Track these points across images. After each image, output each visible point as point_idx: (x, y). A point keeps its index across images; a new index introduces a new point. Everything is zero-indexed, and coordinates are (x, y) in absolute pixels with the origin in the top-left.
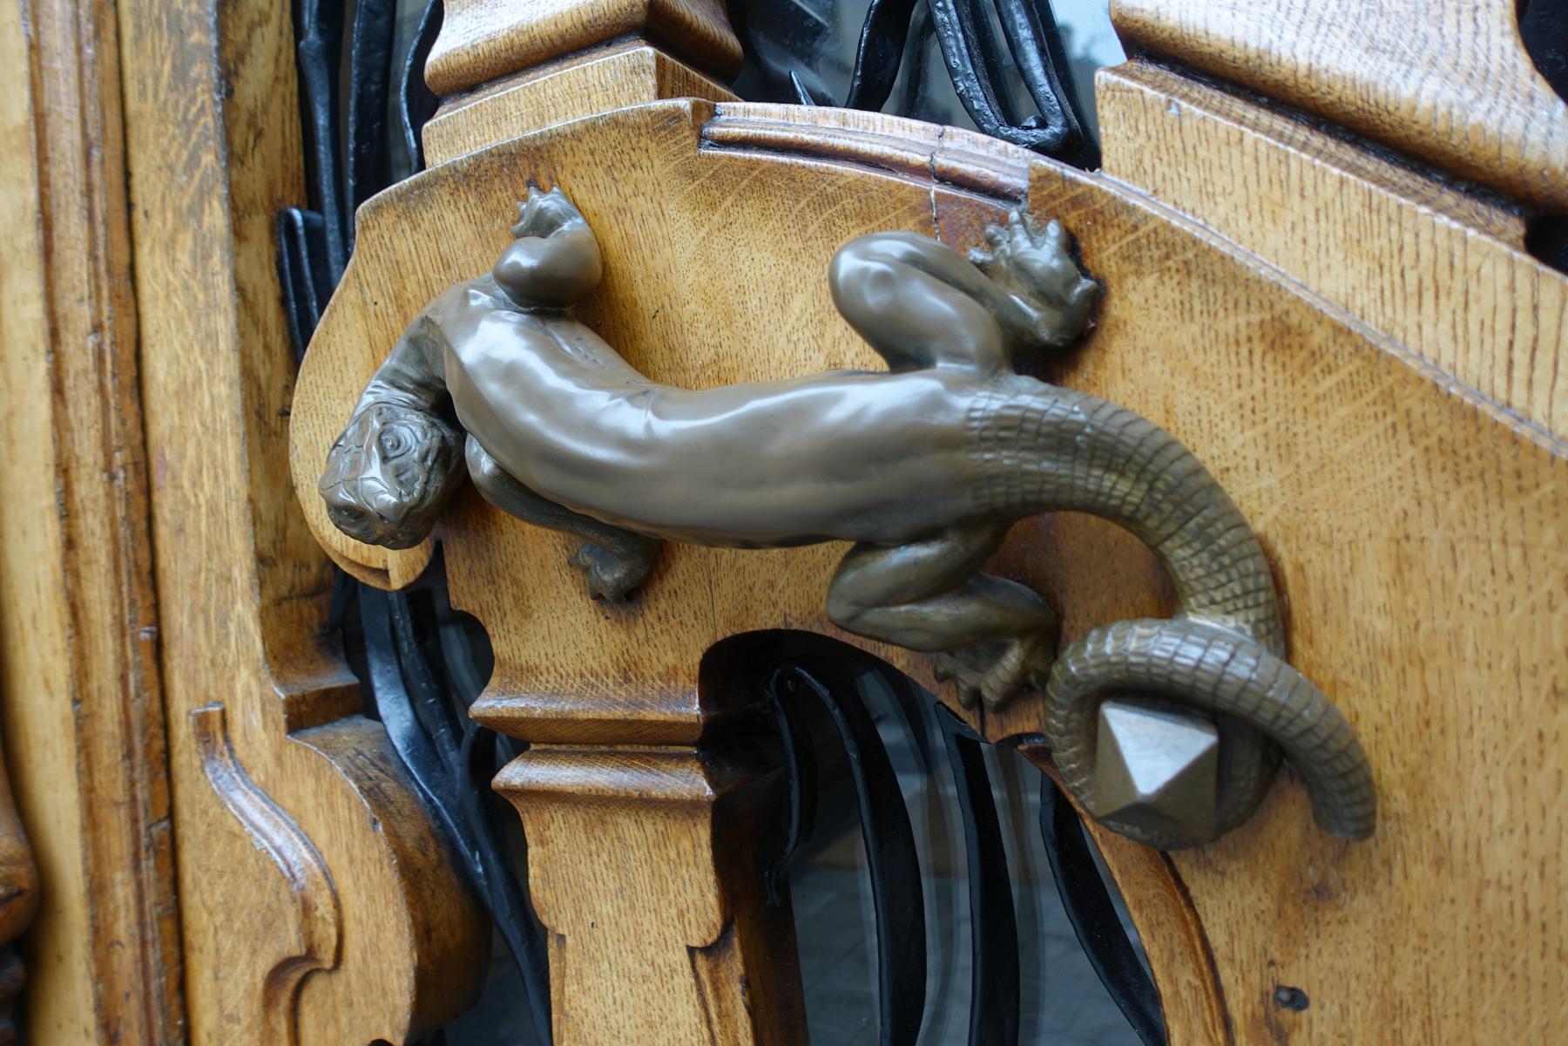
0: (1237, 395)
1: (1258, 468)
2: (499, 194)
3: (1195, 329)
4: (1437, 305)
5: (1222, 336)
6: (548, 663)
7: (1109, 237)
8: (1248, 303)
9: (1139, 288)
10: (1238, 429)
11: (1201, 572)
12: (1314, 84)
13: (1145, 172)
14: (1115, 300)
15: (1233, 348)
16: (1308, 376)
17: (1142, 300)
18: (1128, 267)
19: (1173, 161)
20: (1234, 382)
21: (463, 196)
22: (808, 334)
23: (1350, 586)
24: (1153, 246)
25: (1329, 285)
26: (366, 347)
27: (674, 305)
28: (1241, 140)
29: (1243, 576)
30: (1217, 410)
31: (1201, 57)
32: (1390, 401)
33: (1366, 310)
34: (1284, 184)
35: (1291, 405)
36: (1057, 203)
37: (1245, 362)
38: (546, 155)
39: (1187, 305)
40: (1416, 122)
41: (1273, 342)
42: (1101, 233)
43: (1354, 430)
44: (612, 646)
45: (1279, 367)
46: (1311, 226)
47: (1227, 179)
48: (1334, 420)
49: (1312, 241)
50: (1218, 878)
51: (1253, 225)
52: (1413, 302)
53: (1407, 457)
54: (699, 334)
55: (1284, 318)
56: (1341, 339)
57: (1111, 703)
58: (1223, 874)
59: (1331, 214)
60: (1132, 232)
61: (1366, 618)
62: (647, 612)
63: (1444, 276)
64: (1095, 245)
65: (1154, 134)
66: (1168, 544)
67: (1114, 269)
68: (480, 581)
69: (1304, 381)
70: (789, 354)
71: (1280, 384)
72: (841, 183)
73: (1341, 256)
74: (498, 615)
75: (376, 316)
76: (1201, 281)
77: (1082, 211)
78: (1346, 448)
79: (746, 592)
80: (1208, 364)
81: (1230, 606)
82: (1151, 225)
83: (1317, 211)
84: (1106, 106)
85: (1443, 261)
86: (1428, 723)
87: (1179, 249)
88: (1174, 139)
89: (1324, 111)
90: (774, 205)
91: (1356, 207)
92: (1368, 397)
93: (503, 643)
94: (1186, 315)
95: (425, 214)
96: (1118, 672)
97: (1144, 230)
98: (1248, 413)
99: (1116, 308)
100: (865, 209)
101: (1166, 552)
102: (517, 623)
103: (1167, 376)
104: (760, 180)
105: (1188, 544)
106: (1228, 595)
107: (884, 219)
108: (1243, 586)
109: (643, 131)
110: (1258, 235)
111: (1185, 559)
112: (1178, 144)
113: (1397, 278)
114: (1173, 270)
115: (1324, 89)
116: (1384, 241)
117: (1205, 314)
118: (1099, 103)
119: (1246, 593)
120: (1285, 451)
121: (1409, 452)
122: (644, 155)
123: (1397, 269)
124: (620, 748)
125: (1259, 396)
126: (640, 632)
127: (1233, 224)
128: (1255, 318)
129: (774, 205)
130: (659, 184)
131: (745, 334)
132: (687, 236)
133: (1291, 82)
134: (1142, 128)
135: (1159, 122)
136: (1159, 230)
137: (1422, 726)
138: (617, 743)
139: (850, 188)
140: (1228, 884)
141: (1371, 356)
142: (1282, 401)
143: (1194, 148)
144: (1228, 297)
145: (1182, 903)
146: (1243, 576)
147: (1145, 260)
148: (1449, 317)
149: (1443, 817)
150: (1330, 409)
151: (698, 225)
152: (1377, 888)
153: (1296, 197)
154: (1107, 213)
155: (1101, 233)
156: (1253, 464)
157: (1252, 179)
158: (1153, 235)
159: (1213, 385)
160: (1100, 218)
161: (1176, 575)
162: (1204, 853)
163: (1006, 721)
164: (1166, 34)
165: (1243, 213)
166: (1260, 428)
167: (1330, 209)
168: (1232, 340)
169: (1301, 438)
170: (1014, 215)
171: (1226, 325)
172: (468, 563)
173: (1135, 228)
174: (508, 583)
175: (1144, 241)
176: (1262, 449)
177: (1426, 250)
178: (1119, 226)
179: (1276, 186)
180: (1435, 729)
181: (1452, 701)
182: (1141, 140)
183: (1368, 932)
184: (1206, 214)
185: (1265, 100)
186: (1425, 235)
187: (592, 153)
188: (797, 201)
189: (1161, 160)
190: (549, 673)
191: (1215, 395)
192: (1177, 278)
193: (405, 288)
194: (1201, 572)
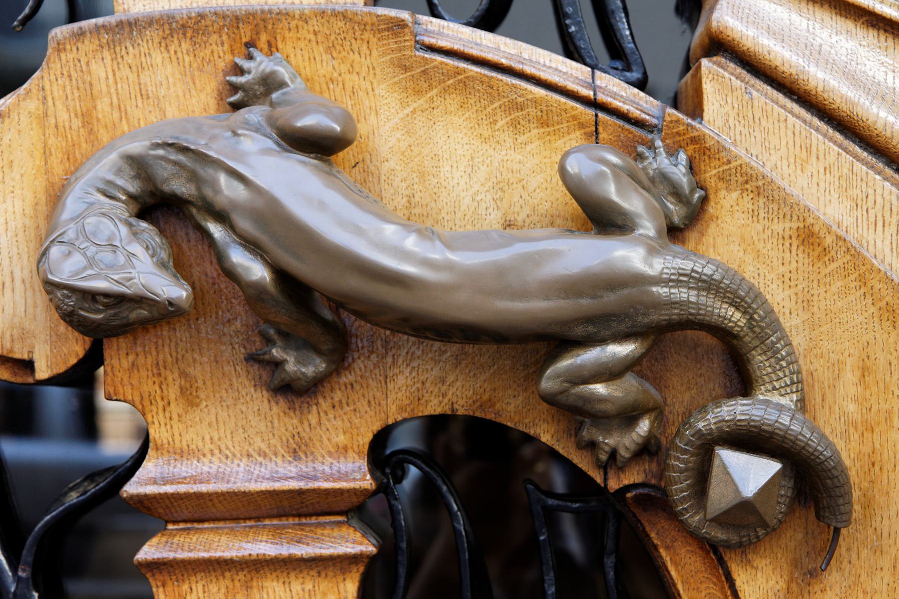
0: (782, 269)
1: (791, 313)
2: (214, 47)
3: (759, 227)
4: (884, 231)
5: (775, 233)
6: (212, 447)
7: (712, 165)
8: (791, 217)
9: (727, 198)
10: (781, 290)
11: (769, 370)
12: (826, 96)
13: (730, 128)
14: (712, 203)
15: (781, 241)
16: (821, 262)
17: (729, 206)
18: (721, 185)
19: (747, 124)
20: (780, 262)
21: (176, 41)
22: (489, 197)
23: (837, 385)
24: (738, 175)
25: (830, 210)
26: (38, 154)
27: (373, 160)
28: (786, 120)
29: (792, 373)
30: (769, 277)
31: (807, 93)
32: (864, 281)
33: (849, 228)
34: (809, 150)
35: (811, 278)
36: (681, 138)
37: (787, 251)
38: (270, 27)
39: (756, 213)
40: (876, 129)
41: (803, 241)
42: (707, 161)
43: (844, 295)
44: (283, 430)
45: (806, 256)
46: (822, 176)
47: (777, 141)
48: (834, 288)
49: (822, 184)
50: (754, 571)
51: (791, 172)
52: (872, 227)
53: (870, 312)
54: (395, 184)
55: (810, 227)
56: (840, 243)
57: (720, 447)
58: (756, 568)
59: (832, 171)
60: (727, 164)
61: (845, 403)
62: (321, 401)
63: (887, 215)
64: (703, 168)
65: (736, 106)
66: (753, 352)
67: (713, 184)
68: (143, 373)
69: (819, 265)
70: (472, 209)
71: (806, 265)
72: (530, 97)
73: (837, 196)
74: (161, 404)
75: (56, 127)
76: (765, 200)
77: (697, 146)
78: (839, 304)
79: (419, 385)
80: (766, 249)
81: (783, 391)
82: (739, 162)
83: (825, 168)
84: (708, 82)
85: (887, 207)
86: (873, 464)
87: (754, 179)
88: (748, 111)
89: (768, 73)
90: (472, 101)
91: (845, 171)
92: (853, 277)
93: (163, 429)
94: (755, 218)
95: (130, 49)
96: (729, 426)
97: (733, 164)
98: (787, 280)
99: (711, 209)
100: (545, 117)
101: (751, 357)
102: (181, 411)
103: (741, 254)
104: (465, 85)
105: (765, 353)
106: (783, 385)
107: (558, 127)
108: (792, 379)
109: (368, 28)
110: (793, 177)
111: (761, 362)
112: (750, 115)
113: (864, 212)
114: (749, 191)
115: (831, 100)
116: (859, 191)
117: (766, 219)
118: (704, 80)
119: (793, 383)
120: (807, 304)
121: (872, 309)
122: (365, 46)
123: (865, 208)
124: (267, 522)
125: (794, 271)
126: (313, 418)
127: (779, 167)
128: (795, 225)
129: (472, 101)
130: (374, 68)
131: (436, 190)
132: (393, 111)
133: (813, 92)
134: (729, 101)
135: (739, 99)
136: (743, 166)
137: (871, 466)
138: (264, 518)
139: (536, 102)
140: (759, 574)
141: (855, 255)
142: (806, 275)
143: (760, 120)
144: (780, 211)
145: (729, 593)
146: (792, 373)
147: (733, 182)
148: (889, 237)
149: (879, 519)
150: (832, 282)
151: (404, 104)
152: (843, 566)
153: (814, 158)
154: (712, 150)
155: (707, 161)
156: (788, 311)
157: (791, 143)
158: (739, 168)
159: (768, 262)
160: (708, 152)
161: (755, 372)
162: (746, 555)
163: (622, 476)
164: (745, 48)
165: (785, 162)
166: (793, 290)
167: (832, 168)
168: (781, 236)
169: (815, 297)
170: (659, 143)
171: (778, 227)
172: (131, 358)
173: (729, 162)
174: (176, 375)
175: (734, 171)
176: (793, 302)
177: (879, 200)
178: (719, 159)
179: (804, 150)
180: (877, 468)
181: (886, 450)
182: (728, 108)
183: (837, 595)
184: (764, 160)
185: (796, 97)
186: (879, 191)
187: (315, 33)
188: (492, 102)
189: (739, 122)
190: (213, 455)
191: (769, 268)
192: (751, 196)
193: (95, 107)
194: (769, 370)
